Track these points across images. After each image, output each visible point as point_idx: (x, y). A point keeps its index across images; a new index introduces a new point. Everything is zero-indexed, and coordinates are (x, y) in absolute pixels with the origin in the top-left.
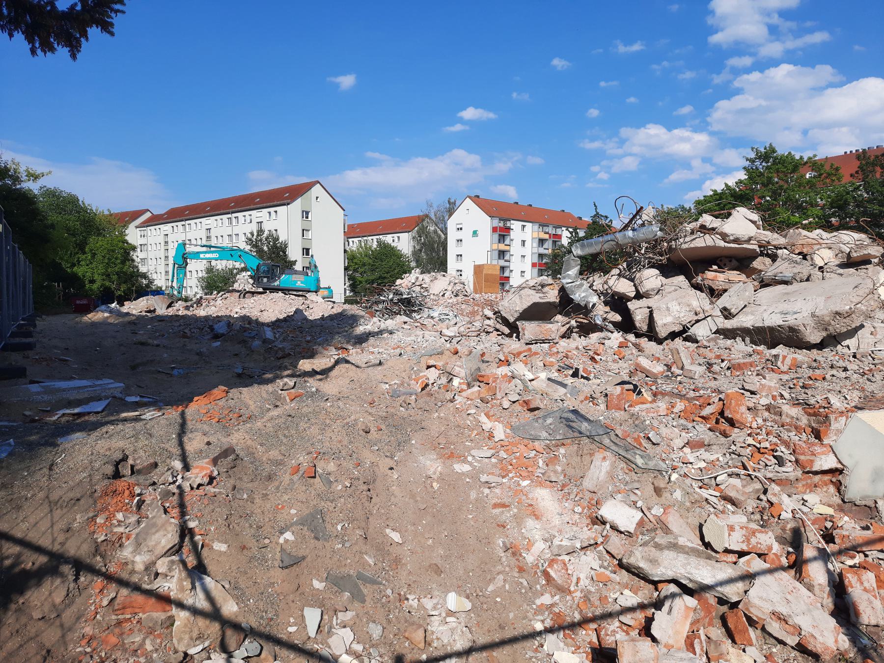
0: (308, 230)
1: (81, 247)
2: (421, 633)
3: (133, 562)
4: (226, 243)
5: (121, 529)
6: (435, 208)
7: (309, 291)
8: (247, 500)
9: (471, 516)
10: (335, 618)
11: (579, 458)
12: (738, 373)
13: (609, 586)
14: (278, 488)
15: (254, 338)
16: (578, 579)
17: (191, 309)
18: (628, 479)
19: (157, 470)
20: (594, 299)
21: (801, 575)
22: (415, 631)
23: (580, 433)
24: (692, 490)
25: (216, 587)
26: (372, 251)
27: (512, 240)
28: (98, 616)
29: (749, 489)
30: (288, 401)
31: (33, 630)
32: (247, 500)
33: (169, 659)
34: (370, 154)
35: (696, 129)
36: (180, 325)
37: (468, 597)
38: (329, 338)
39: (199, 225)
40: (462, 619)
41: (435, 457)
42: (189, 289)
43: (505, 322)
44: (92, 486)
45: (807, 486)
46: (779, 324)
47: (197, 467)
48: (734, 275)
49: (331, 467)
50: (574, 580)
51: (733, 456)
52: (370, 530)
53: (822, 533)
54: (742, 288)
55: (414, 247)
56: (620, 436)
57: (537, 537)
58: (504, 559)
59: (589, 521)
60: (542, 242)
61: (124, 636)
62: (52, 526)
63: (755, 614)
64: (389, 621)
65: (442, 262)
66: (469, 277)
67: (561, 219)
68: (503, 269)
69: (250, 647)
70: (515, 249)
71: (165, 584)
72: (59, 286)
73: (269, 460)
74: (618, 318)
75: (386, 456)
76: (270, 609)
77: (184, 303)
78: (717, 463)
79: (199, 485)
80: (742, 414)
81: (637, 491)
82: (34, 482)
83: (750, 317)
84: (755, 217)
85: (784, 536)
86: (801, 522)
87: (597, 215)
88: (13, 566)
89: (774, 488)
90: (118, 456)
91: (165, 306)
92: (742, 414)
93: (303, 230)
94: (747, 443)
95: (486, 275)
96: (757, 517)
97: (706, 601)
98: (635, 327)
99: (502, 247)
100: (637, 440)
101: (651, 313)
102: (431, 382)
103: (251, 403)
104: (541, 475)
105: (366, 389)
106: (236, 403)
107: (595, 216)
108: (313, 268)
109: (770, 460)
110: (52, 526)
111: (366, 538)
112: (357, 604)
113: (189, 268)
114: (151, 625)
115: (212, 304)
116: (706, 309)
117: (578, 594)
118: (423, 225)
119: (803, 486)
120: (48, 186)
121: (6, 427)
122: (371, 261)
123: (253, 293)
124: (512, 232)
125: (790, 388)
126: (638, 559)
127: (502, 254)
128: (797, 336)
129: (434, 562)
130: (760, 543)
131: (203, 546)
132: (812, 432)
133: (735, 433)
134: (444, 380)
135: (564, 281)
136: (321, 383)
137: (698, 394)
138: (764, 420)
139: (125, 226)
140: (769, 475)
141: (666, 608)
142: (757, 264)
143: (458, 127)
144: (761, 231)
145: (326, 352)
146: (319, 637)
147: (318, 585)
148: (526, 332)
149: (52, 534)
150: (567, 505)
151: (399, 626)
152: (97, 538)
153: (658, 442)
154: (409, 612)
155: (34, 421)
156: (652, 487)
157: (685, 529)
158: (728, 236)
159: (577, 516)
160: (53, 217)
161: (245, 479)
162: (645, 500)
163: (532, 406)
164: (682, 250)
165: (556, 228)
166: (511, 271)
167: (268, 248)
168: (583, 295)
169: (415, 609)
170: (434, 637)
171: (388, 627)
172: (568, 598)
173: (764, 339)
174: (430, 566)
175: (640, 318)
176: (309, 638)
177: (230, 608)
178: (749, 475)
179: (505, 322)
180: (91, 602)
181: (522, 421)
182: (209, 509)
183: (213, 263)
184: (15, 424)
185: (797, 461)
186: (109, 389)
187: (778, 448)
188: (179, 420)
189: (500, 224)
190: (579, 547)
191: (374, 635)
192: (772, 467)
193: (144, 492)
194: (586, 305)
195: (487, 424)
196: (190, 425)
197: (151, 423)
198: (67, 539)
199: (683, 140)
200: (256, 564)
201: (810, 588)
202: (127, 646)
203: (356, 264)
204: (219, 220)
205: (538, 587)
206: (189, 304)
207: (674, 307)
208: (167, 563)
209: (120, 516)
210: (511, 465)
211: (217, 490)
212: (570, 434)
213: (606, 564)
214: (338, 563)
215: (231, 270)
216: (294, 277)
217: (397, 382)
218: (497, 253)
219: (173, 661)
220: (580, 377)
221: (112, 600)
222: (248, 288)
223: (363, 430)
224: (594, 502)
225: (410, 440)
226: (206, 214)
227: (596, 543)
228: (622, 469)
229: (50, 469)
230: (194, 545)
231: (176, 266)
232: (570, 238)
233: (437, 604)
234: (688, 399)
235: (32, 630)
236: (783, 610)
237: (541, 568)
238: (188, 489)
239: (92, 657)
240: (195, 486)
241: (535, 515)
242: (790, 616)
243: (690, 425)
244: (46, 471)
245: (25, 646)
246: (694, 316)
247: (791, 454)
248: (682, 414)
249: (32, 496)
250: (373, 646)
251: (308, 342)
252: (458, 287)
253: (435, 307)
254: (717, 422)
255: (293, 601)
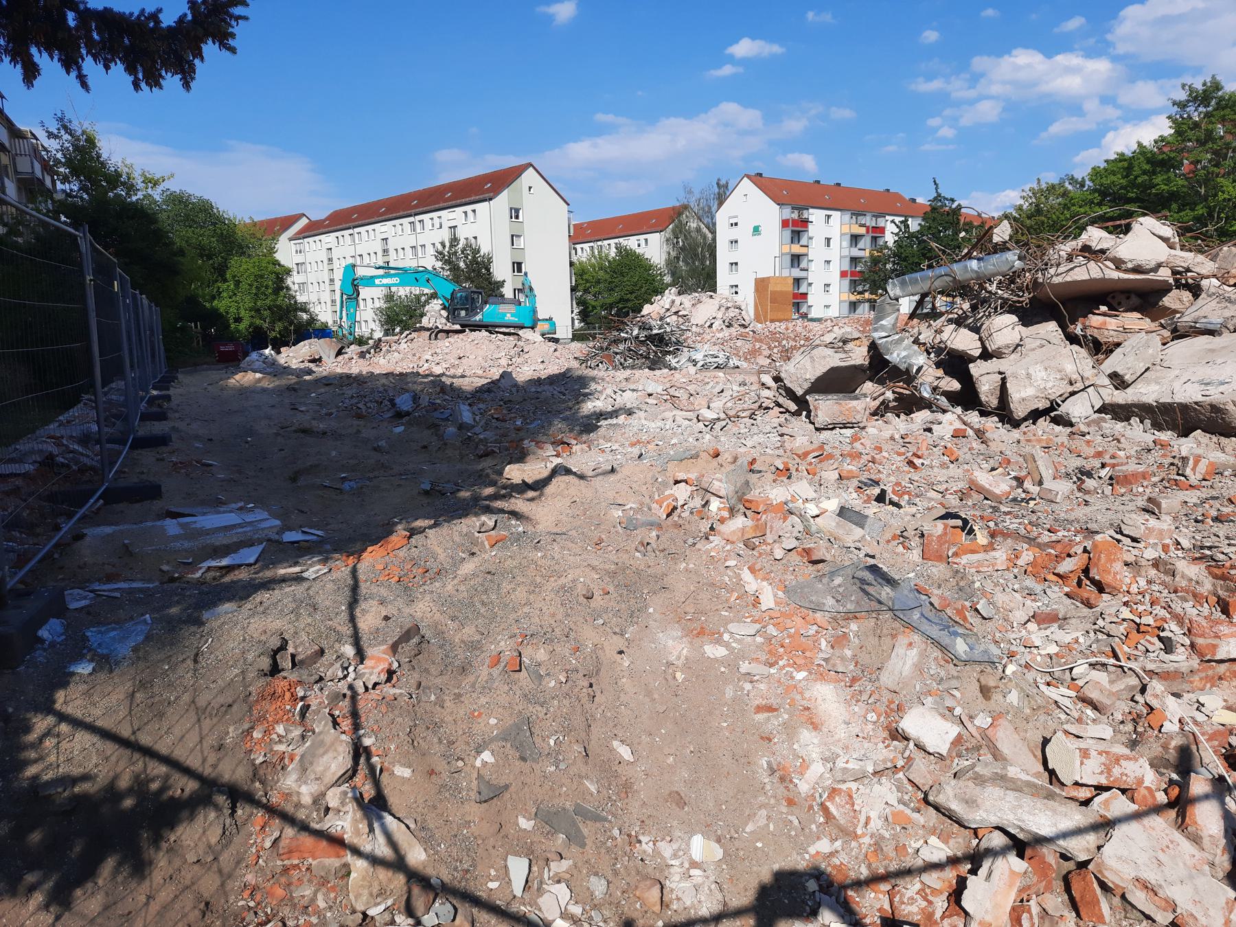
0: (519, 236)
1: (221, 271)
2: (656, 892)
3: (299, 793)
4: (409, 262)
5: (281, 748)
6: (697, 195)
7: (522, 327)
8: (436, 704)
9: (725, 724)
10: (546, 869)
11: (877, 639)
12: (1123, 490)
13: (910, 831)
14: (473, 686)
15: (447, 419)
16: (868, 819)
17: (368, 356)
18: (943, 674)
19: (324, 659)
20: (920, 360)
21: (1183, 821)
22: (649, 888)
23: (880, 602)
24: (1035, 691)
25: (399, 828)
26: (609, 261)
27: (811, 238)
28: (261, 861)
29: (1120, 685)
30: (487, 547)
31: (189, 876)
32: (436, 704)
33: (345, 920)
34: (601, 117)
35: (1090, 54)
36: (352, 397)
37: (718, 841)
38: (546, 424)
39: (371, 233)
40: (710, 872)
41: (680, 634)
42: (363, 323)
43: (790, 394)
44: (246, 687)
45: (1208, 679)
46: (1196, 400)
47: (373, 658)
48: (1132, 319)
49: (542, 655)
50: (863, 819)
51: (1100, 636)
52: (592, 742)
53: (1224, 751)
54: (1143, 341)
55: (669, 253)
56: (936, 605)
57: (814, 755)
58: (768, 787)
59: (886, 734)
60: (855, 239)
61: (293, 888)
62: (201, 742)
63: (1110, 878)
64: (616, 873)
65: (708, 274)
66: (747, 298)
67: (885, 203)
68: (797, 281)
69: (442, 908)
70: (816, 251)
71: (338, 823)
72: (196, 327)
73: (463, 641)
74: (955, 385)
75: (615, 633)
76: (466, 858)
77: (357, 347)
78: (1076, 646)
79: (375, 684)
80: (1116, 574)
81: (955, 692)
82: (177, 679)
83: (1154, 388)
84: (1168, 231)
85: (1166, 757)
86: (1192, 737)
87: (938, 197)
88: (163, 789)
89: (1156, 686)
90: (275, 643)
91: (333, 353)
92: (1116, 574)
93: (512, 236)
94: (1121, 616)
95: (773, 293)
96: (1129, 727)
97: (1043, 861)
98: (980, 403)
99: (796, 249)
100: (960, 612)
101: (1004, 380)
102: (680, 503)
103: (439, 551)
104: (823, 663)
105: (591, 517)
106: (420, 552)
107: (935, 199)
108: (527, 290)
109: (1154, 644)
110: (201, 742)
111: (587, 755)
112: (575, 849)
113: (361, 297)
114: (322, 874)
115: (394, 348)
116: (1086, 375)
117: (867, 840)
118: (680, 221)
119: (1201, 679)
120: (172, 189)
121: (140, 590)
122: (607, 277)
123: (448, 332)
124: (810, 226)
125: (1197, 521)
126: (949, 797)
127: (796, 259)
128: (1223, 419)
129: (676, 789)
130: (1126, 775)
131: (381, 770)
132: (1218, 603)
133: (1106, 602)
134: (697, 502)
135: (876, 335)
136: (533, 505)
137: (1054, 538)
138: (1149, 582)
139: (273, 239)
140: (1150, 666)
141: (983, 871)
142: (1168, 301)
143: (727, 70)
144: (1178, 252)
145: (540, 452)
146: (527, 896)
147: (525, 824)
148: (820, 413)
149: (202, 752)
150: (856, 709)
151: (628, 880)
152: (254, 759)
153: (991, 616)
154: (642, 860)
155: (172, 580)
156: (977, 684)
157: (1020, 749)
158: (1124, 263)
159: (870, 726)
160: (180, 236)
161: (433, 670)
162: (966, 704)
163: (814, 558)
164: (1052, 286)
165: (877, 217)
166: (810, 284)
167: (466, 264)
168: (904, 354)
169: (649, 855)
170: (674, 896)
171: (614, 881)
172: (854, 844)
173: (1174, 420)
174: (670, 794)
175: (987, 389)
176: (515, 897)
177: (416, 856)
178: (1121, 667)
179: (790, 394)
180: (252, 842)
181: (800, 579)
182: (387, 719)
183: (393, 289)
184: (151, 586)
185: (1193, 646)
186: (263, 529)
187: (1166, 626)
188: (350, 582)
189: (793, 216)
190: (871, 771)
191: (597, 893)
192: (1155, 654)
193: (308, 693)
194: (907, 369)
195: (751, 583)
196: (364, 588)
197: (317, 586)
198: (219, 760)
199: (1069, 70)
200: (447, 794)
201: (1196, 839)
202: (296, 901)
203: (587, 281)
204: (398, 226)
205: (813, 827)
206: (364, 348)
207: (1039, 373)
208: (338, 795)
209: (280, 729)
210: (782, 646)
211: (397, 691)
212: (866, 603)
213: (906, 797)
214: (550, 793)
215: (418, 298)
216: (503, 308)
217: (633, 506)
218: (788, 258)
219: (349, 923)
220: (887, 502)
221: (276, 841)
222: (442, 323)
223: (584, 595)
224: (894, 706)
225: (646, 607)
226: (380, 218)
227: (895, 767)
228: (936, 659)
229: (196, 661)
230: (372, 768)
231: (345, 297)
232: (897, 234)
233: (679, 849)
234: (1039, 546)
235: (187, 876)
236: (1151, 876)
237: (818, 799)
238: (361, 690)
239: (256, 913)
240: (370, 687)
241: (812, 723)
242: (1160, 886)
243: (1038, 588)
244: (190, 662)
245: (181, 897)
246: (1068, 386)
247: (1184, 634)
248: (1030, 569)
249: (176, 698)
250: (595, 907)
251: (519, 430)
252: (732, 313)
253: (698, 346)
254: (1079, 584)
255: (494, 847)
